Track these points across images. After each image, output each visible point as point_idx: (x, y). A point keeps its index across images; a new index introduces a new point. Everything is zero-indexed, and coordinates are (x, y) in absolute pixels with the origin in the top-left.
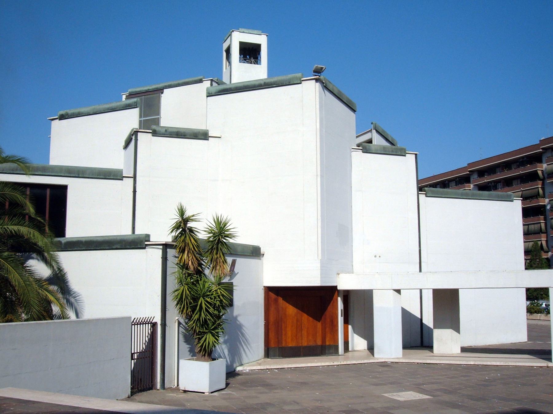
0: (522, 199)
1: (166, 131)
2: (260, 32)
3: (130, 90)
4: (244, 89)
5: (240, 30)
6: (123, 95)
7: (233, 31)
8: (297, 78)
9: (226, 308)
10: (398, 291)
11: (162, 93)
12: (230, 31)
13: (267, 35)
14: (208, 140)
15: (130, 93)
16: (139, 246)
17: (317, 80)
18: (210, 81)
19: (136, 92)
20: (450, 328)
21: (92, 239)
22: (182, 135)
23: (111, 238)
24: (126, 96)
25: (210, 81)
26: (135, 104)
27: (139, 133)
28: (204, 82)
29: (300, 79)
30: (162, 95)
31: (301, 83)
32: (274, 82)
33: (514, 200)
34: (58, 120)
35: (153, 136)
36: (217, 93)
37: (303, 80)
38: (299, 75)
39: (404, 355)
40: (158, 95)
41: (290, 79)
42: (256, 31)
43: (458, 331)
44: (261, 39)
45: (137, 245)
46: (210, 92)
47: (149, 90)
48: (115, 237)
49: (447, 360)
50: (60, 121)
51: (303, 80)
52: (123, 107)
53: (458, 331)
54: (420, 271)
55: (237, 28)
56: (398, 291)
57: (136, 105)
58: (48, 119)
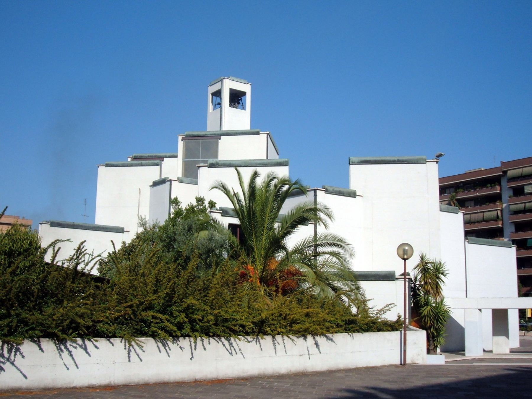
0: (221, 212)
1: (333, 190)
2: (246, 82)
3: (187, 133)
4: (381, 162)
5: (231, 78)
6: (179, 137)
7: (225, 78)
8: (423, 159)
9: (17, 318)
10: (480, 310)
11: (220, 139)
12: (220, 77)
13: (251, 85)
14: (355, 197)
15: (186, 135)
16: (391, 279)
17: (437, 162)
18: (266, 134)
19: (193, 135)
20: (503, 336)
21: (377, 273)
22: (342, 194)
23: (367, 273)
24: (182, 137)
25: (266, 134)
26: (286, 163)
27: (317, 191)
28: (260, 134)
29: (426, 160)
30: (219, 141)
31: (425, 163)
32: (405, 160)
33: (309, 224)
34: (207, 167)
35: (325, 193)
36: (359, 162)
37: (427, 161)
38: (424, 157)
39: (483, 354)
40: (216, 140)
41: (418, 159)
42: (243, 80)
43: (508, 337)
44: (245, 88)
45: (389, 279)
46: (353, 162)
47: (206, 135)
48: (370, 273)
49: (498, 356)
50: (209, 168)
51: (427, 161)
52: (274, 164)
53: (508, 337)
54: (467, 297)
55: (228, 76)
56: (480, 310)
57: (287, 164)
58: (197, 165)
